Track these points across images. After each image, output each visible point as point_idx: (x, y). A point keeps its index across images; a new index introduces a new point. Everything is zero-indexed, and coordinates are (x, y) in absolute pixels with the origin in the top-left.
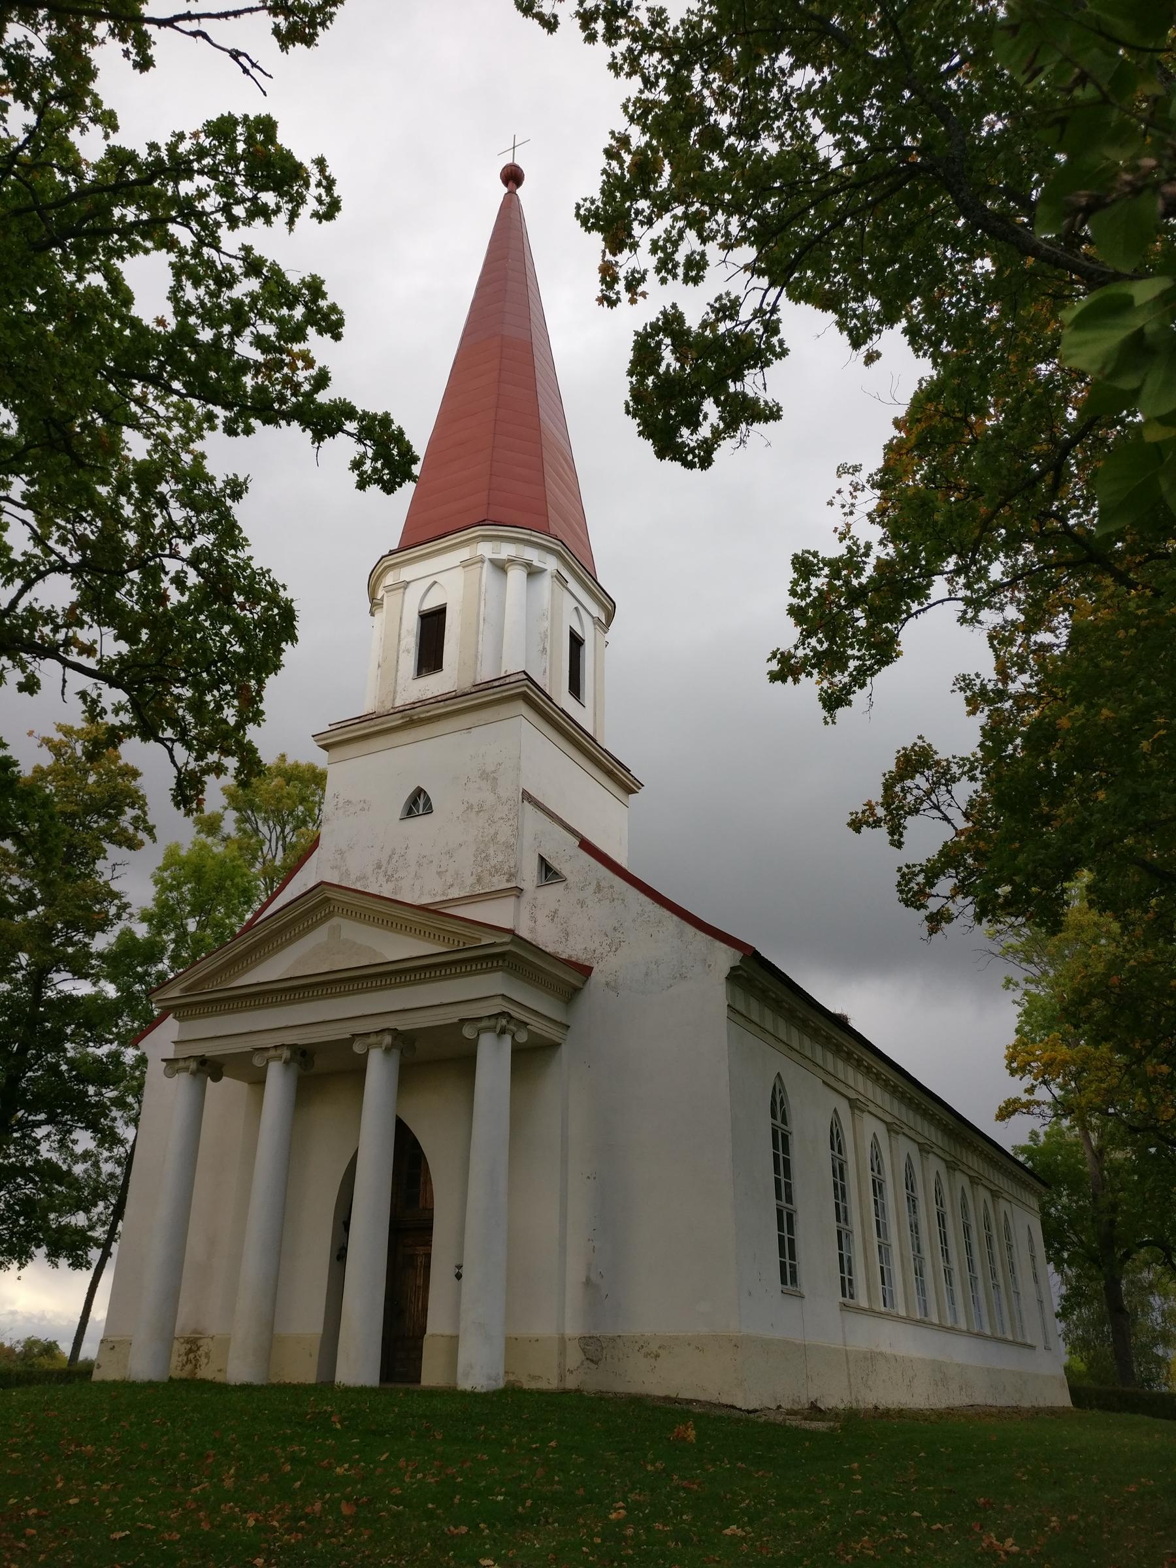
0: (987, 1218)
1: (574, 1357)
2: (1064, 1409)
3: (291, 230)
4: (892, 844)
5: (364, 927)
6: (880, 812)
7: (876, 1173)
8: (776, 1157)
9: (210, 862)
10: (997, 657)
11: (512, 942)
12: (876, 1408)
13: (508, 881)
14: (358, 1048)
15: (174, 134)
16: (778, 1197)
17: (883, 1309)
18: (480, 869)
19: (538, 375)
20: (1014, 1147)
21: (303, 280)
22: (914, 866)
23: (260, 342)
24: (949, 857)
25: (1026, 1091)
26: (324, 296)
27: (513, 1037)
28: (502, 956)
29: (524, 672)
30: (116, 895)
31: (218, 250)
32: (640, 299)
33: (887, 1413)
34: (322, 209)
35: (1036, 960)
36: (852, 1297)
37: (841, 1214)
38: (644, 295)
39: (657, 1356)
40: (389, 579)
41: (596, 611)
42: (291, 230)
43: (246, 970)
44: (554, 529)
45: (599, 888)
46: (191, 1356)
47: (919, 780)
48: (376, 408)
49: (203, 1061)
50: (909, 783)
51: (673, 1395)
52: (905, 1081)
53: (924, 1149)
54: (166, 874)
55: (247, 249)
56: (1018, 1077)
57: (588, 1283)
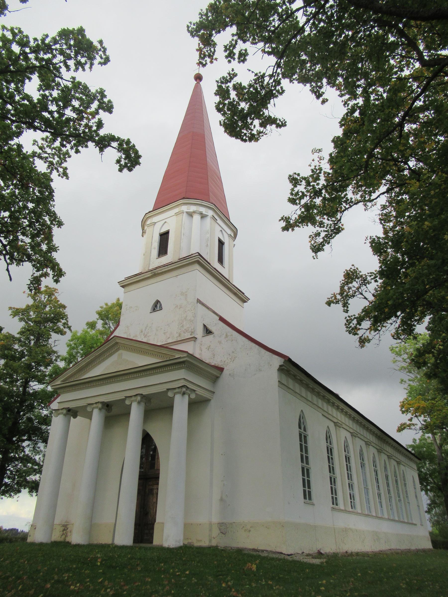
0: (395, 472)
1: (216, 532)
2: (429, 550)
3: (91, 70)
4: (344, 312)
5: (131, 353)
6: (339, 297)
7: (346, 453)
8: (301, 445)
9: (88, 338)
10: (384, 228)
11: (187, 356)
12: (346, 552)
13: (191, 335)
14: (127, 402)
15: (44, 35)
16: (302, 461)
17: (351, 510)
18: (180, 331)
19: (206, 146)
20: (407, 445)
21: (97, 91)
22: (352, 316)
23: (74, 109)
24: (366, 313)
25: (409, 420)
26: (105, 96)
27: (189, 396)
28: (183, 362)
29: (198, 253)
30: (55, 352)
31: (62, 78)
32: (214, 61)
33: (352, 554)
34: (103, 61)
35: (413, 372)
36: (337, 505)
37: (331, 469)
38: (216, 59)
39: (250, 531)
40: (149, 222)
41: (229, 232)
42: (91, 70)
43: (85, 373)
44: (212, 200)
45: (227, 336)
46: (65, 532)
47: (354, 284)
48: (124, 137)
49: (69, 410)
50: (350, 285)
51: (256, 548)
52: (361, 418)
53: (368, 444)
54: (72, 343)
55: (74, 78)
56: (405, 414)
57: (222, 500)
